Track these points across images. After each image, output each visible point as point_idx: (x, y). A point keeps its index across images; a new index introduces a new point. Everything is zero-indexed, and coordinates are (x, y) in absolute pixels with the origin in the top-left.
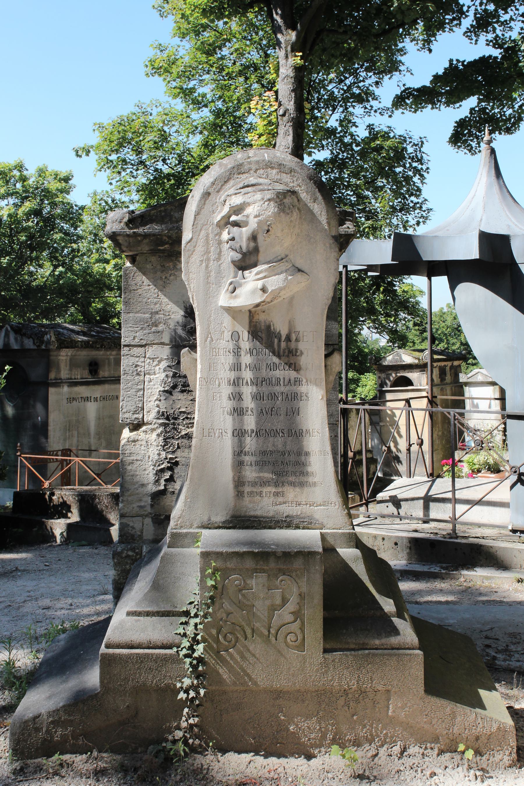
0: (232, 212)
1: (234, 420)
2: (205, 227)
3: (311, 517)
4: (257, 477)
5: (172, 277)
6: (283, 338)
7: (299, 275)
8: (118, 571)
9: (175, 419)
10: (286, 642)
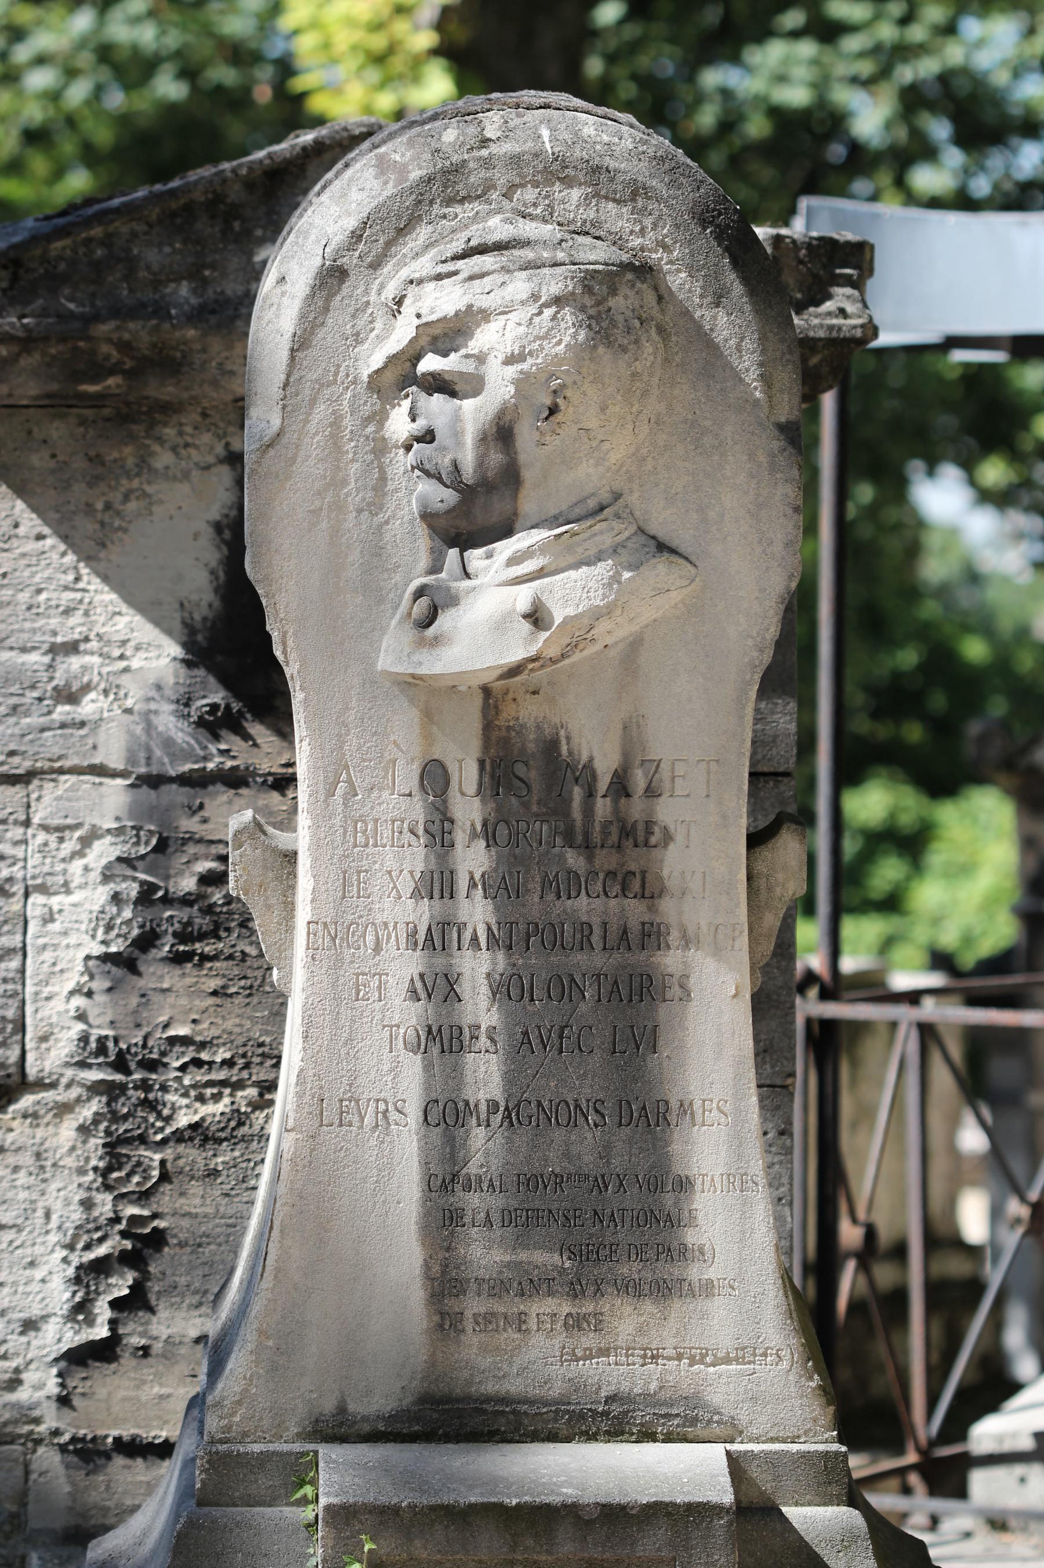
0: (424, 341)
1: (428, 1067)
2: (327, 392)
3: (694, 1401)
4: (508, 1265)
5: (132, 505)
6: (603, 784)
7: (660, 568)
9: (151, 1065)
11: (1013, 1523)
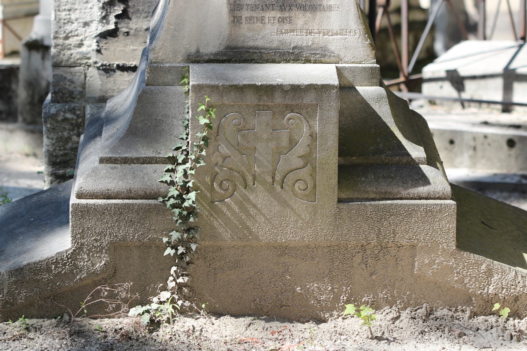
8: (52, 139)
10: (293, 191)
11: (438, 102)
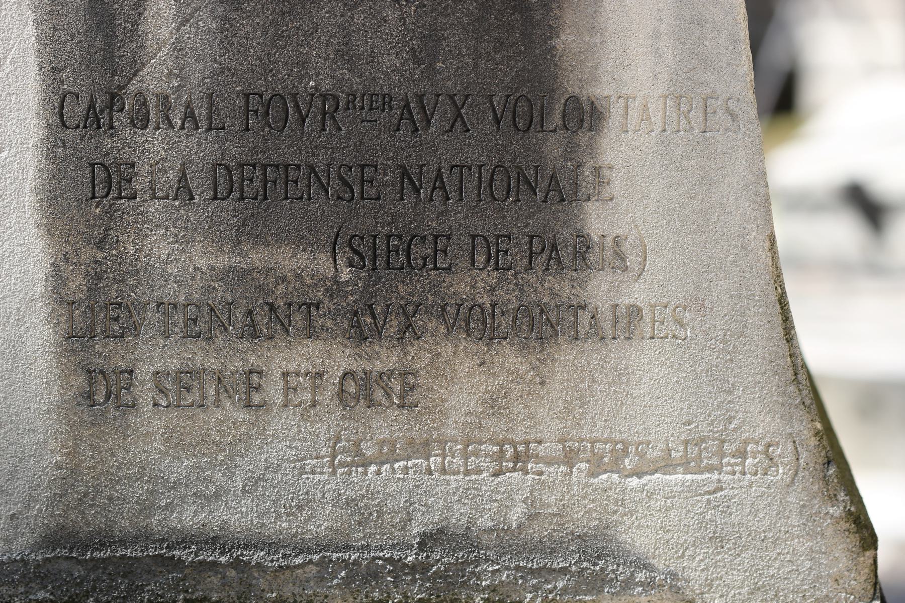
4: (227, 275)
